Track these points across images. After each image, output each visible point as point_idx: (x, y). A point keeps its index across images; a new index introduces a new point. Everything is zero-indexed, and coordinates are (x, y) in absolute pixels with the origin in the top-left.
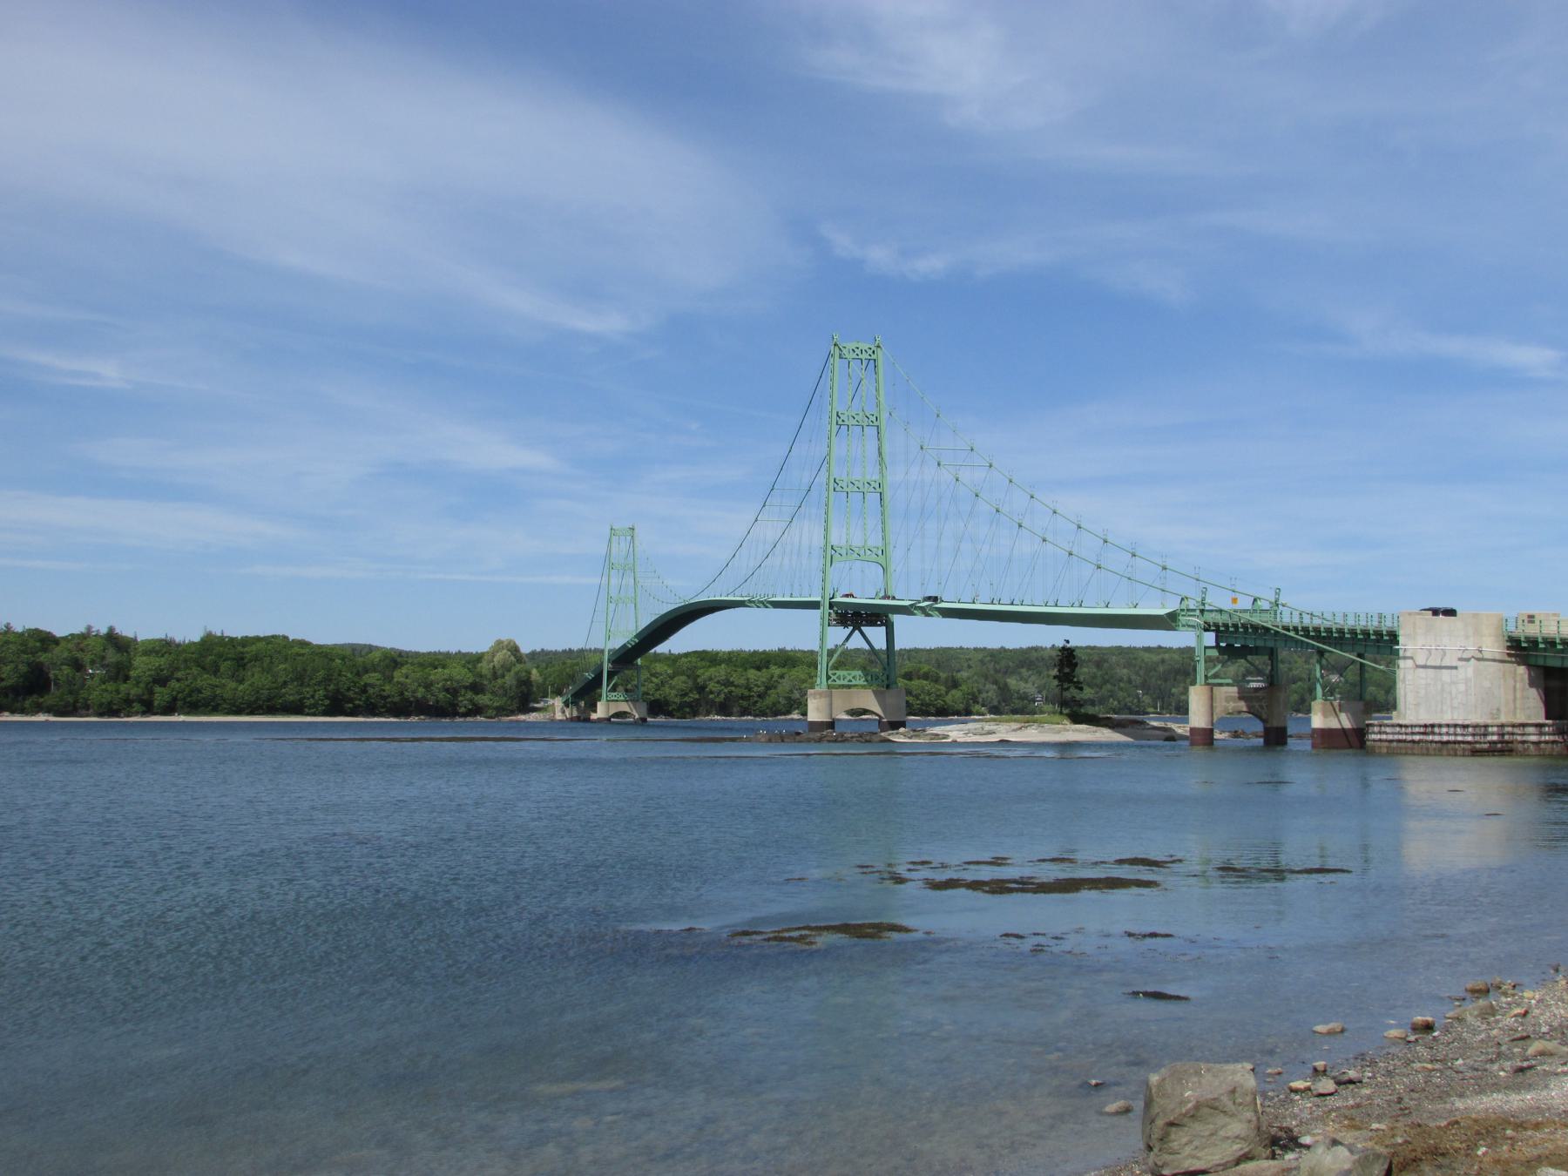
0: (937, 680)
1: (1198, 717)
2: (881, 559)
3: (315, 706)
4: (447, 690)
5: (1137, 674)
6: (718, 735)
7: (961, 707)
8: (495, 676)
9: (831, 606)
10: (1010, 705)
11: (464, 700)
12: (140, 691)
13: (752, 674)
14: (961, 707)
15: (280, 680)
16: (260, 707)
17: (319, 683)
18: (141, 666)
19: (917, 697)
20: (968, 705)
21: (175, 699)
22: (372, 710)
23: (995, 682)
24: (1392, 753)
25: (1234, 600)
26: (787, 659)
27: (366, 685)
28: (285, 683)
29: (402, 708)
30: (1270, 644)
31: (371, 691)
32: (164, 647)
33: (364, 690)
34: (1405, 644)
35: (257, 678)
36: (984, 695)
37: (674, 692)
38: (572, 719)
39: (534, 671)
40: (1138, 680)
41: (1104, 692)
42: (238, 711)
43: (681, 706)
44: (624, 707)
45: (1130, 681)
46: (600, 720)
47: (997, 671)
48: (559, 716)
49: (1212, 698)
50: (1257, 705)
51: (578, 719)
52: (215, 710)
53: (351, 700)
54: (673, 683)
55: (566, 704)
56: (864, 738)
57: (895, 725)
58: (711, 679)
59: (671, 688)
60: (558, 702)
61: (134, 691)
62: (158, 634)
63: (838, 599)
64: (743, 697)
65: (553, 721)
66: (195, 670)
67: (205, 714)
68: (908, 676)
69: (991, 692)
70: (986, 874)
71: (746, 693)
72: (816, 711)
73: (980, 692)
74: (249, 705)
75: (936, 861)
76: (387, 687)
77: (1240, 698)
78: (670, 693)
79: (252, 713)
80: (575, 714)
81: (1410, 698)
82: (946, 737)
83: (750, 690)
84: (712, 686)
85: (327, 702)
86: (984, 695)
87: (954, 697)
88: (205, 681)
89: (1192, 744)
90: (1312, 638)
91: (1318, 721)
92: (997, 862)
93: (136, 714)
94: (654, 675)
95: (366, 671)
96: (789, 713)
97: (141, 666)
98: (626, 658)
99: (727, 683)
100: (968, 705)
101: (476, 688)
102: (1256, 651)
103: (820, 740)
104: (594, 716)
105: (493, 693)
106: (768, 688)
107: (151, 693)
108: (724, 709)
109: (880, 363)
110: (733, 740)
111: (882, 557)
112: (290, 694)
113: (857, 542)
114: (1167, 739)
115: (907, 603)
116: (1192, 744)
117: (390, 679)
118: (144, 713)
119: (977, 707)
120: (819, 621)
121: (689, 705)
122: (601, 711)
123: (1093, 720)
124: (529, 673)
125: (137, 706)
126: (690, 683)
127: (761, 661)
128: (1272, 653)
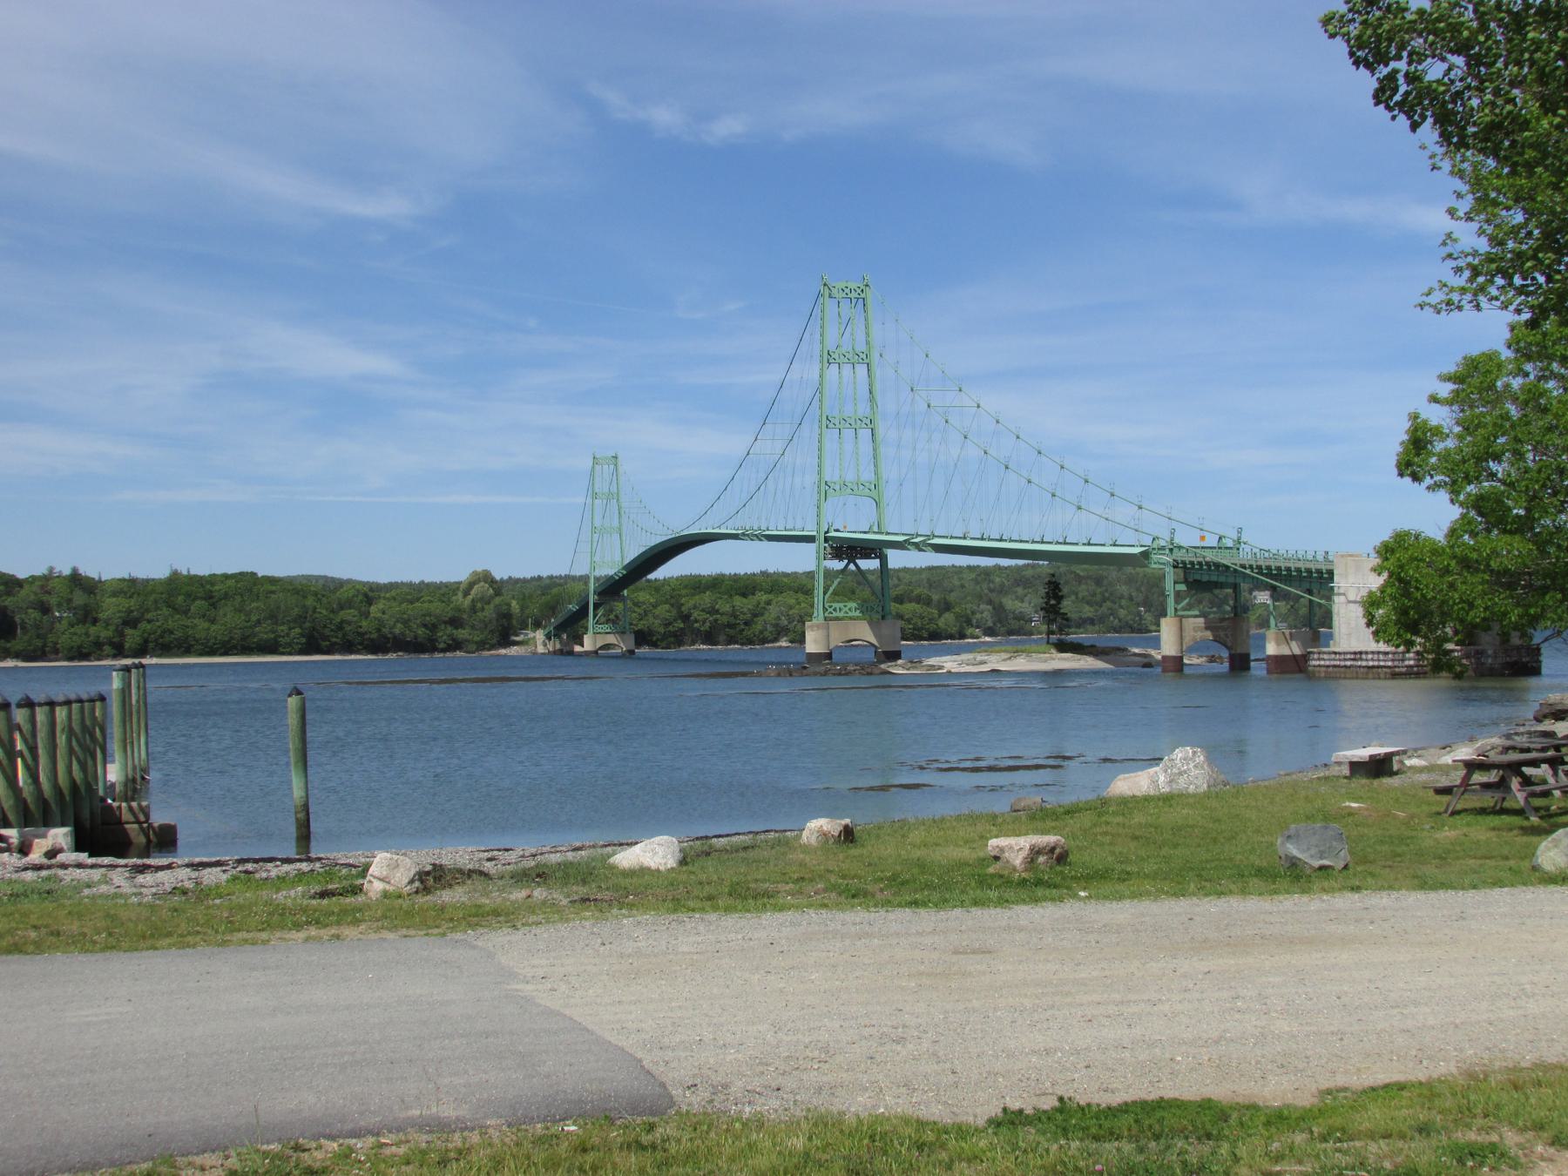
0: (928, 602)
1: (1168, 644)
2: (874, 494)
3: (290, 645)
4: (425, 626)
5: (1138, 590)
6: (743, 669)
7: (954, 630)
8: (473, 609)
9: (826, 540)
10: (1007, 628)
11: (444, 634)
12: (110, 633)
13: (738, 601)
14: (954, 630)
15: (254, 618)
16: (235, 647)
17: (295, 621)
18: (111, 608)
19: (909, 621)
20: (962, 628)
21: (146, 641)
22: (348, 648)
23: (990, 602)
24: (1329, 677)
25: (1202, 538)
26: (774, 584)
27: (342, 622)
28: (259, 622)
29: (379, 645)
30: (1231, 580)
31: (348, 628)
32: (131, 587)
33: (340, 627)
34: (1339, 582)
35: (229, 620)
36: (978, 616)
37: (657, 622)
38: (555, 652)
39: (514, 603)
40: (1140, 598)
41: (1104, 609)
42: (212, 652)
43: (665, 636)
44: (611, 639)
45: (1131, 599)
46: (587, 653)
47: (991, 591)
48: (541, 649)
49: (1181, 629)
50: (1222, 634)
51: (561, 652)
52: (187, 652)
53: (326, 638)
54: (657, 611)
55: (548, 637)
56: (866, 669)
57: (894, 656)
58: (695, 607)
59: (656, 617)
60: (540, 635)
61: (105, 634)
62: (123, 573)
63: (833, 534)
64: (730, 626)
65: (535, 653)
66: (165, 611)
67: (177, 656)
68: (900, 600)
69: (986, 613)
70: (968, 764)
71: (732, 620)
72: (813, 644)
73: (973, 613)
74: (224, 644)
75: (943, 759)
76: (364, 623)
77: (1207, 628)
78: (656, 624)
79: (226, 654)
80: (558, 646)
81: (1344, 630)
82: (941, 668)
83: (736, 617)
84: (695, 614)
85: (304, 640)
86: (978, 616)
87: (947, 621)
88: (175, 622)
89: (1164, 671)
90: (1266, 575)
91: (1271, 649)
92: (977, 759)
93: (107, 657)
94: (637, 604)
95: (342, 608)
96: (776, 640)
97: (111, 608)
98: (612, 589)
99: (713, 611)
100: (962, 628)
101: (455, 622)
102: (1220, 585)
103: (825, 674)
104: (577, 648)
105: (473, 627)
106: (755, 615)
107: (122, 635)
108: (710, 638)
109: (869, 302)
110: (744, 675)
111: (875, 492)
112: (263, 633)
113: (850, 477)
114: (1145, 666)
115: (901, 538)
116: (1164, 671)
117: (366, 615)
118: (115, 657)
119: (969, 631)
120: (814, 555)
121: (674, 635)
122: (589, 643)
123: (1077, 648)
124: (509, 605)
125: (107, 649)
126: (674, 612)
127: (745, 586)
128: (1235, 587)
